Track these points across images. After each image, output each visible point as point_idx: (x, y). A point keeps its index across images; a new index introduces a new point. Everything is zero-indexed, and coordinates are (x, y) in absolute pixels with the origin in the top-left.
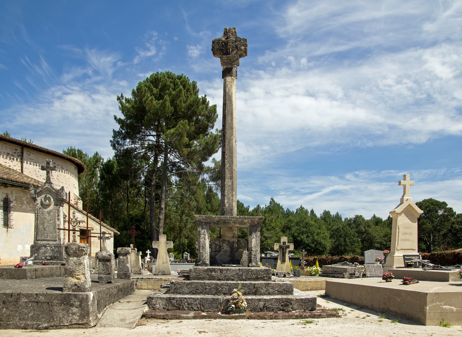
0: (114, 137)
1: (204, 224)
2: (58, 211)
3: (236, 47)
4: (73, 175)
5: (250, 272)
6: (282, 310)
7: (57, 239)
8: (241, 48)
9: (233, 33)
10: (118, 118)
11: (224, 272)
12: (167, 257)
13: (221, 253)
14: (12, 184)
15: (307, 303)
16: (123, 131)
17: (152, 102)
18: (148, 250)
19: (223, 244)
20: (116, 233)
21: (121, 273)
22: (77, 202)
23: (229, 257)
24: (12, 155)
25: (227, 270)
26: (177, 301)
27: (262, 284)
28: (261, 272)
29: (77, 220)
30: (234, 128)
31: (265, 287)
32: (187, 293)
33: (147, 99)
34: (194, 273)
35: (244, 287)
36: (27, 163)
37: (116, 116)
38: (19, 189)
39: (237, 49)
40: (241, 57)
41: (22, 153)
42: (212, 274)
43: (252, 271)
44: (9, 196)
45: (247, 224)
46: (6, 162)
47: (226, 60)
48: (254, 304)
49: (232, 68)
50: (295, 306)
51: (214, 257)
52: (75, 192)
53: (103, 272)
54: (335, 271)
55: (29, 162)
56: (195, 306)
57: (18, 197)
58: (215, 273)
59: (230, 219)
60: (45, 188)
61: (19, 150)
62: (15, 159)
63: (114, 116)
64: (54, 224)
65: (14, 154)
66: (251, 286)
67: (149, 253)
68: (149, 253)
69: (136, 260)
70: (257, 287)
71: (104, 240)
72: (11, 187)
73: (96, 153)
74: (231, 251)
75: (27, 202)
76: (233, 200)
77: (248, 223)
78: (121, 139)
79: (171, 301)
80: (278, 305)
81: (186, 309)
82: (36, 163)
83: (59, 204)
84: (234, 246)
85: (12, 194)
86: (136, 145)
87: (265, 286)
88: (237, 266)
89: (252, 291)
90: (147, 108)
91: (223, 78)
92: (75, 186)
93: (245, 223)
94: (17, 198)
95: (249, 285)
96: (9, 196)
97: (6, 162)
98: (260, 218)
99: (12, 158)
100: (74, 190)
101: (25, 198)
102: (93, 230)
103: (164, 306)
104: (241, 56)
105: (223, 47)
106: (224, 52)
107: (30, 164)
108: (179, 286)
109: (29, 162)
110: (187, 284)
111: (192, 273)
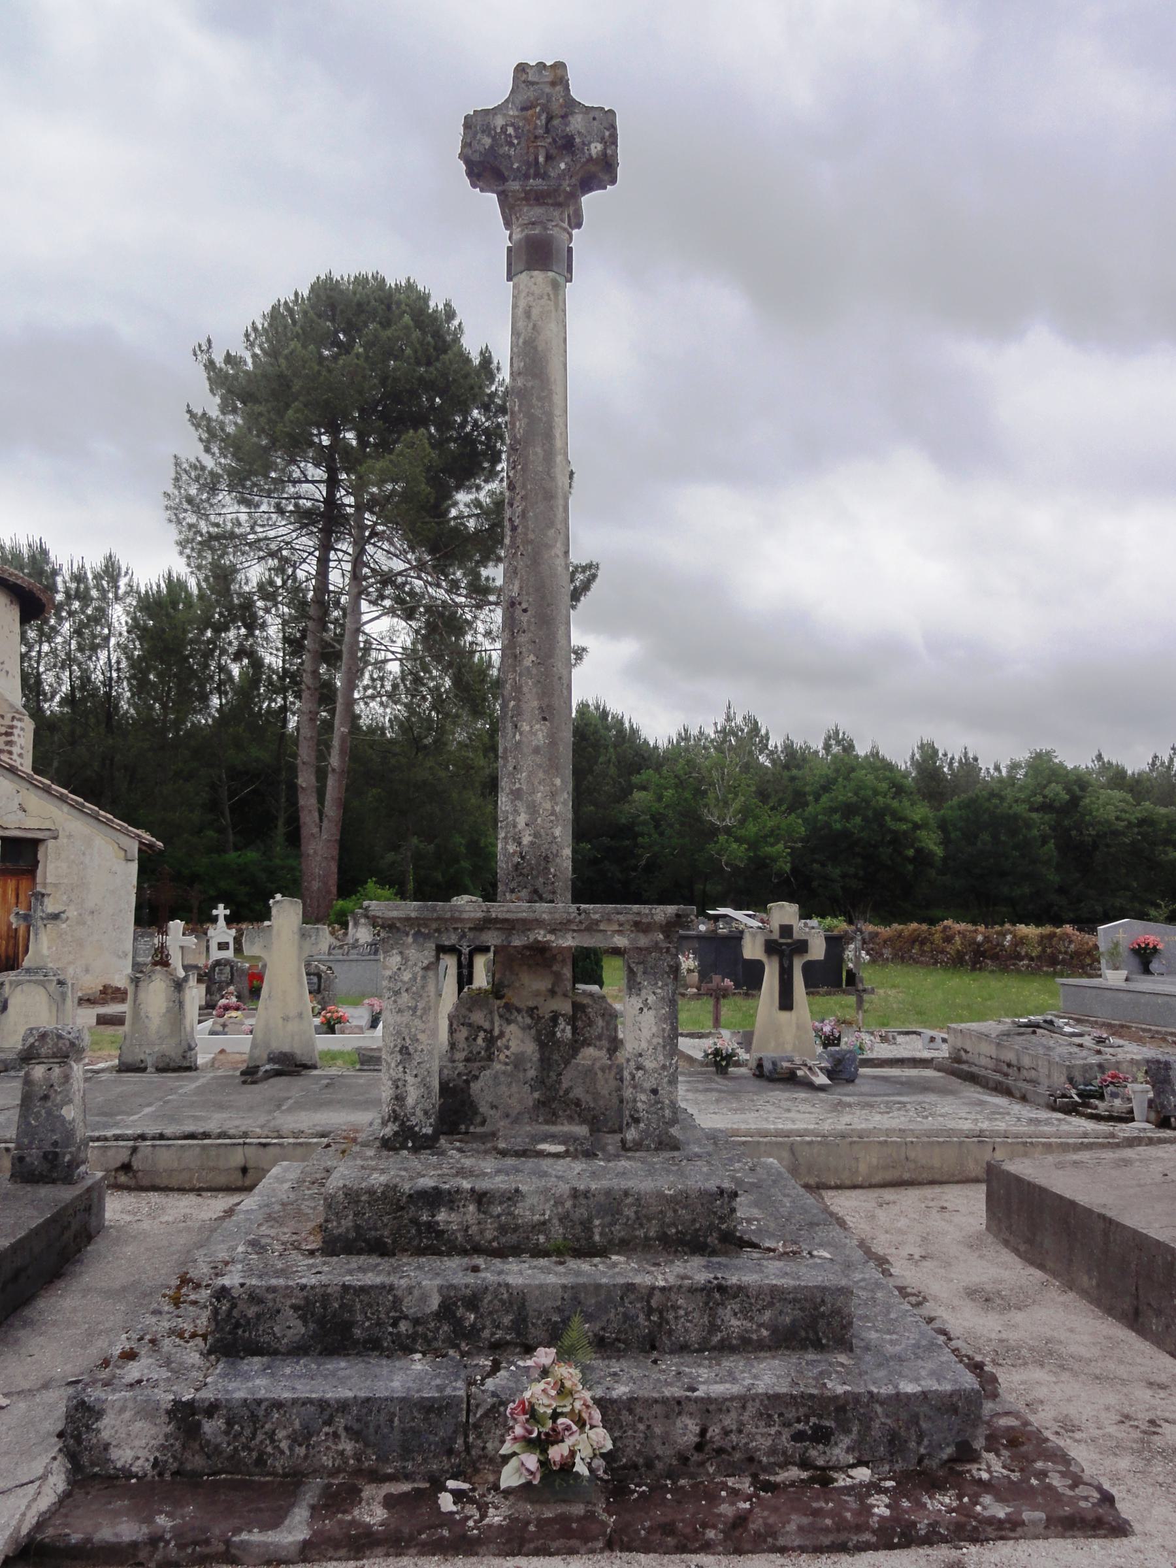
12: (301, 996)
13: (497, 1066)
18: (221, 906)
20: (151, 846)
23: (533, 1089)
40: (590, 190)
48: (649, 1427)
51: (462, 1090)
54: (1009, 1065)
68: (226, 916)
69: (168, 1010)
74: (541, 1060)
84: (559, 1034)
88: (567, 1151)
91: (509, 279)
92: (6, 667)
102: (55, 838)
104: (589, 183)
105: (511, 144)
106: (516, 166)
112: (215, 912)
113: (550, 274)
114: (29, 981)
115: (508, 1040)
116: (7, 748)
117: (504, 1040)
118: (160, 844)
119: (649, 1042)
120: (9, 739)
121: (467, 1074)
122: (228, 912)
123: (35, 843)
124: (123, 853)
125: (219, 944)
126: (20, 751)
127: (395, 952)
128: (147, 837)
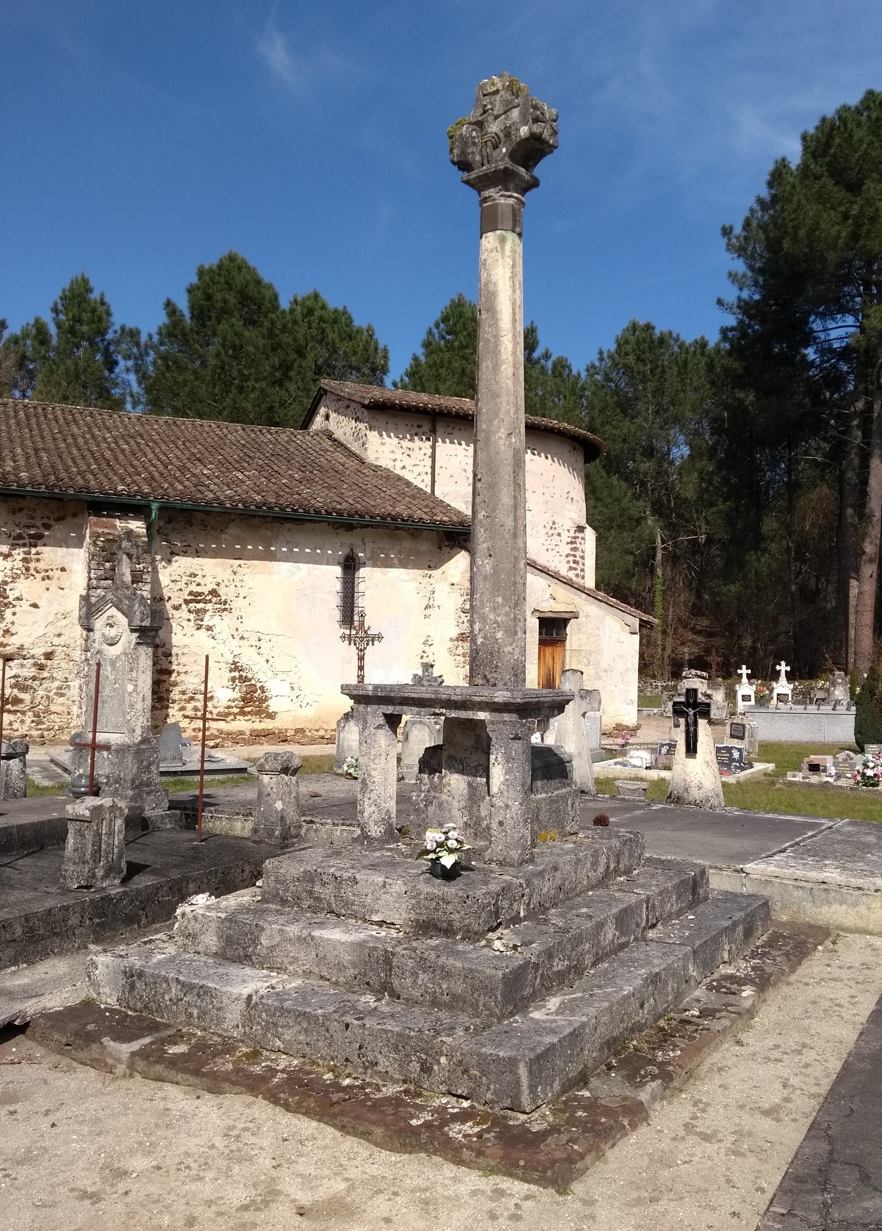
18: (783, 663)
29: (369, 632)
46: (395, 460)
67: (786, 671)
68: (786, 671)
97: (395, 460)
102: (577, 618)
113: (498, 232)
116: (573, 553)
120: (573, 546)
122: (749, 671)
123: (564, 622)
125: (743, 696)
126: (581, 554)
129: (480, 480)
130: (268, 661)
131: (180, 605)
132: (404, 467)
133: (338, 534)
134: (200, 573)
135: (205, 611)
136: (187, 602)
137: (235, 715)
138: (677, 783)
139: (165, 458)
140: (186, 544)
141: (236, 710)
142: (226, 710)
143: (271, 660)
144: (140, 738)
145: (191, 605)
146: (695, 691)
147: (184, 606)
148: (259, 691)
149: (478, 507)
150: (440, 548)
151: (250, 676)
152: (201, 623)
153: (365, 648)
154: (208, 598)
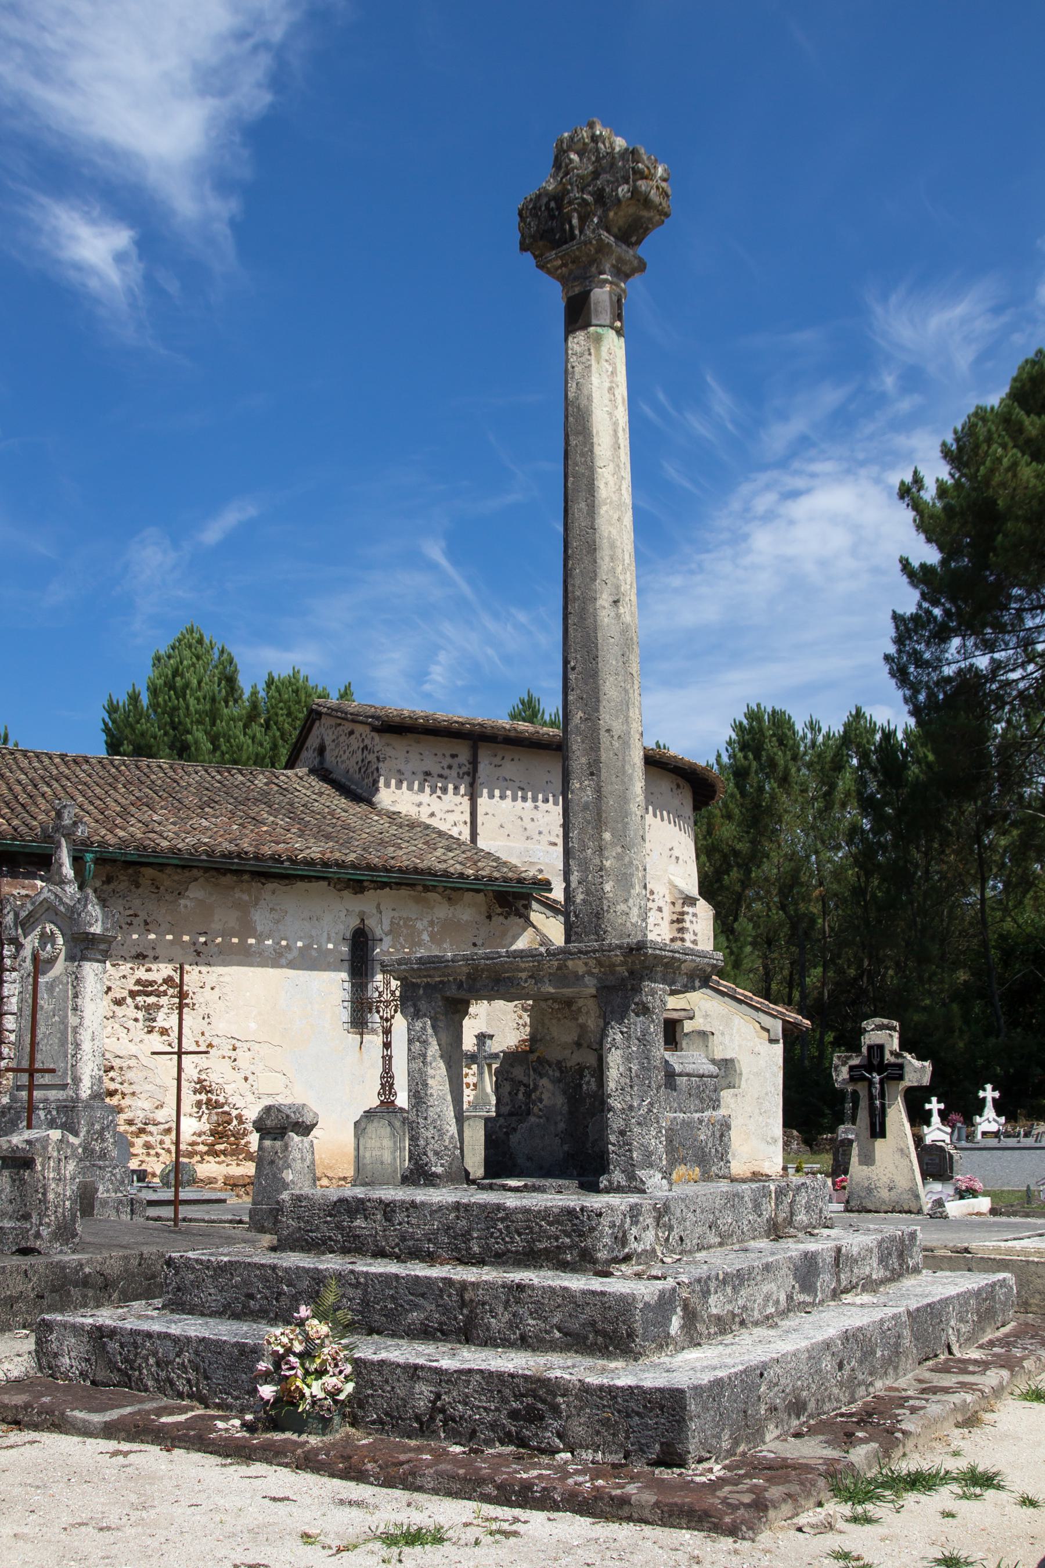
0: (899, 641)
1: (421, 992)
2: (77, 977)
3: (596, 201)
4: (665, 813)
5: (502, 1220)
6: (518, 1438)
7: (69, 1081)
8: (617, 194)
9: (584, 144)
10: (915, 564)
11: (400, 1217)
13: (532, 1119)
14: (369, 878)
15: (638, 1414)
16: (937, 612)
17: (1015, 476)
18: (934, 1099)
19: (538, 1078)
20: (795, 1025)
21: (261, 1209)
22: (683, 913)
24: (441, 776)
25: (411, 1210)
26: (122, 1346)
27: (490, 1286)
28: (550, 1224)
30: (604, 545)
31: (507, 1304)
32: (216, 1312)
33: (992, 471)
34: (293, 1219)
35: (423, 1295)
36: (491, 796)
37: (907, 560)
38: (404, 892)
39: (604, 204)
41: (474, 763)
42: (355, 1224)
43: (509, 1214)
44: (366, 922)
45: (587, 978)
46: (420, 805)
47: (560, 267)
48: (393, 1388)
49: (590, 291)
50: (578, 1429)
52: (671, 877)
53: (10, 1209)
55: (497, 793)
56: (179, 1376)
57: (401, 923)
58: (366, 1218)
59: (511, 963)
60: (41, 902)
61: (464, 756)
62: (451, 787)
63: (901, 561)
64: (62, 1027)
65: (446, 772)
66: (450, 1296)
70: (472, 1301)
71: (483, 1068)
72: (375, 889)
73: (854, 713)
74: (570, 1113)
75: (432, 936)
76: (601, 870)
77: (590, 973)
78: (928, 644)
79: (105, 1343)
80: (497, 1409)
81: (150, 1383)
82: (522, 789)
83: (79, 954)
84: (585, 1087)
85: (381, 913)
86: (996, 656)
87: (507, 1301)
89: (456, 1318)
90: (1000, 502)
93: (576, 974)
94: (398, 924)
95: (441, 1290)
96: (371, 923)
97: (420, 805)
98: (632, 950)
99: (439, 785)
100: (672, 868)
101: (425, 923)
102: (691, 1018)
103: (83, 1364)
107: (503, 797)
108: (192, 1277)
109: (497, 793)
110: (215, 1270)
111: (284, 1219)
112: (927, 1106)
114: (475, 1116)
115: (542, 1093)
116: (680, 935)
117: (538, 1093)
118: (808, 1022)
119: (618, 1082)
120: (680, 925)
121: (506, 1127)
124: (766, 1034)
126: (693, 938)
127: (409, 1003)
128: (793, 1017)
129: (573, 669)
130: (246, 1079)
131: (124, 999)
132: (432, 815)
133: (342, 898)
134: (151, 953)
135: (159, 1007)
136: (133, 994)
137: (202, 1155)
138: (857, 1184)
139: (99, 802)
140: (131, 912)
141: (203, 1148)
142: (190, 1149)
143: (251, 1078)
144: (89, 1092)
145: (138, 999)
146: (881, 1048)
147: (129, 1000)
148: (235, 1122)
149: (572, 707)
150: (489, 917)
151: (222, 1100)
152: (154, 1024)
153: (392, 1017)
154: (162, 989)
